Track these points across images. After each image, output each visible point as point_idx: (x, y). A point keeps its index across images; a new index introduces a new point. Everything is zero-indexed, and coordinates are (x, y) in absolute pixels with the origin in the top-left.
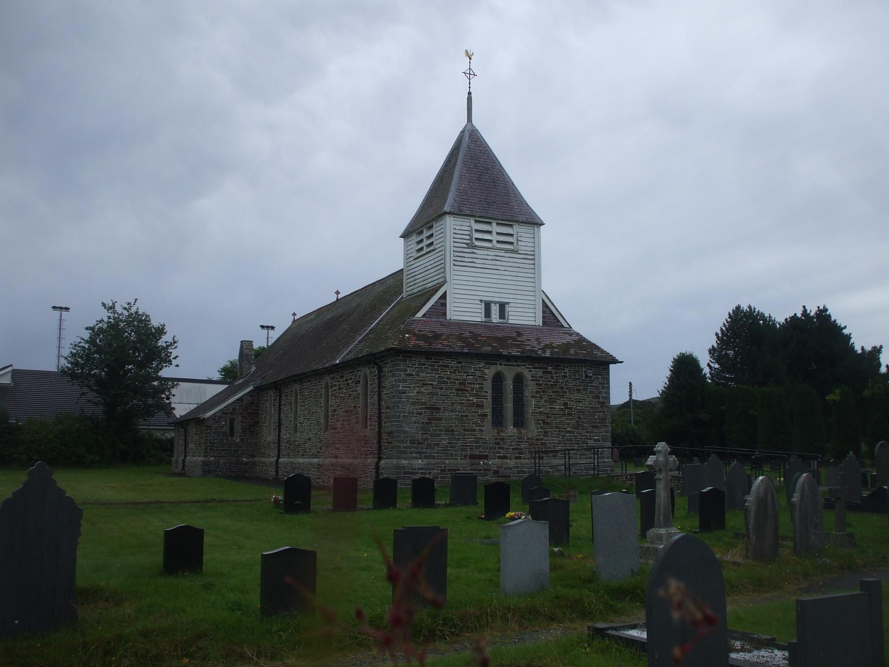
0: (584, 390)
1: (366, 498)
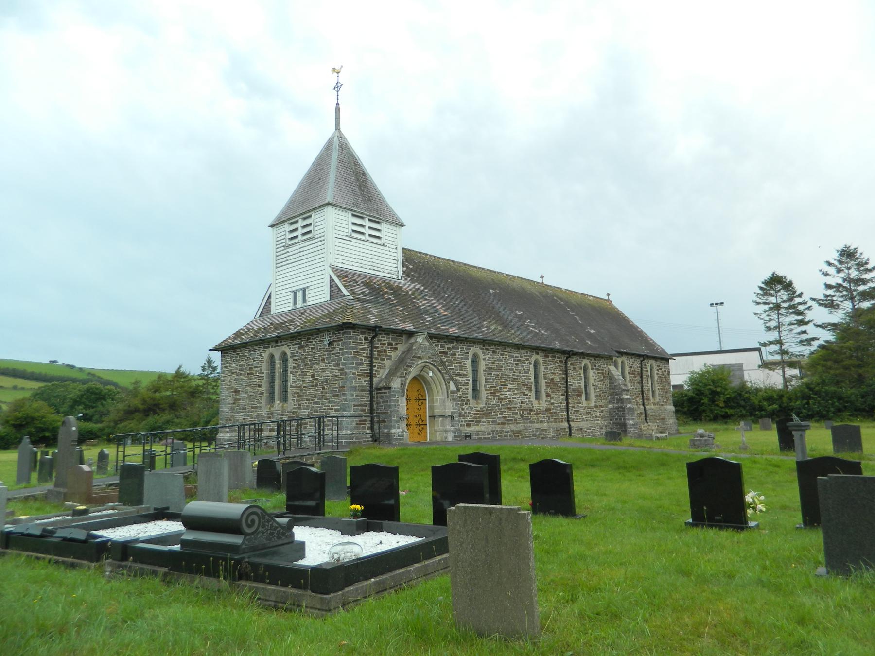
0: (327, 359)
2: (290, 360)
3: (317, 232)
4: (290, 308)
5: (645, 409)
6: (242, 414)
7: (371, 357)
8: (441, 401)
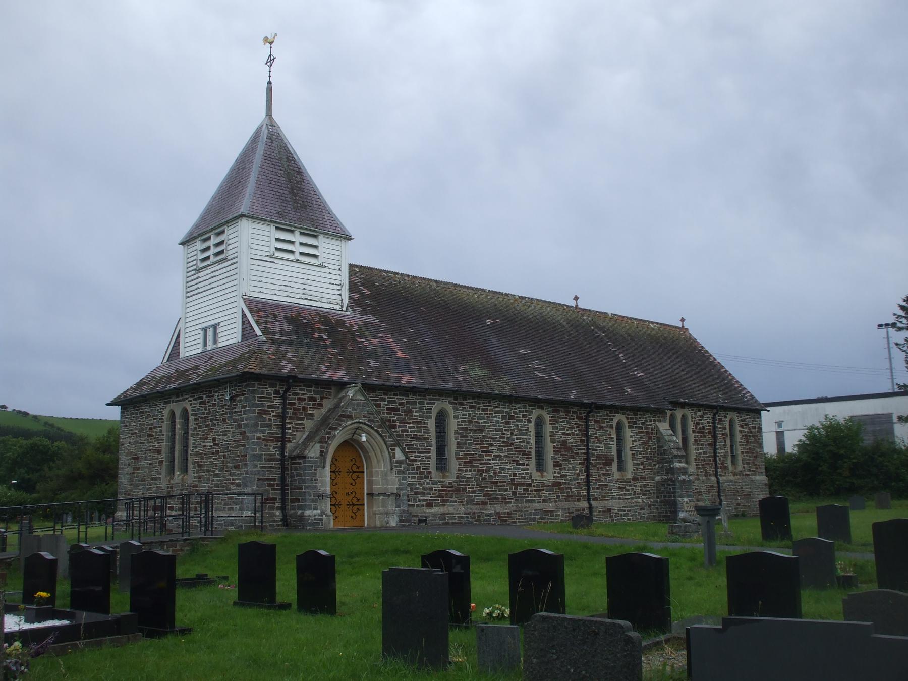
1: (286, 583)
2: (191, 419)
3: (230, 253)
4: (199, 351)
5: (718, 482)
6: (141, 487)
7: (283, 416)
8: (383, 473)
